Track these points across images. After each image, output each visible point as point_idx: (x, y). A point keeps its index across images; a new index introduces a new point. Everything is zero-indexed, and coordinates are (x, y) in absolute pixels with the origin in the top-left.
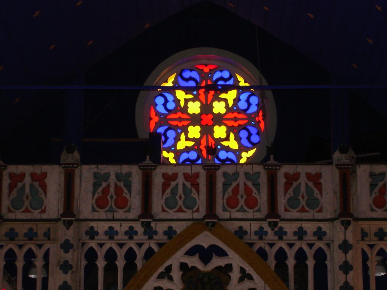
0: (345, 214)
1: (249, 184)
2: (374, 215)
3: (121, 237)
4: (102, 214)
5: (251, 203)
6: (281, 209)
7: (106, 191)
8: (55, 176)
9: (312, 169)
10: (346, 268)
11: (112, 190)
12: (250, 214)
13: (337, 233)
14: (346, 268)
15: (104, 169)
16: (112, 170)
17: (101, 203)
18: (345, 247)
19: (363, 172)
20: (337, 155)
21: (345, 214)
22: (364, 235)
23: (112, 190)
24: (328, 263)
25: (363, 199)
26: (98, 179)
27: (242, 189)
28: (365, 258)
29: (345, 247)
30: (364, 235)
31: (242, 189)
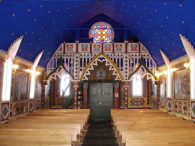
0: (126, 52)
1: (135, 46)
2: (131, 52)
3: (146, 56)
4: (132, 52)
5: (136, 50)
6: (141, 51)
7: (84, 48)
8: (124, 45)
9: (135, 44)
10: (126, 61)
11: (134, 48)
12: (135, 52)
13: (125, 55)
14: (126, 61)
15: (132, 44)
16: (134, 44)
17: (132, 50)
18: (126, 58)
19: (130, 44)
20: (125, 41)
21: (126, 52)
22: (130, 55)
23: (134, 48)
24: (123, 60)
25: (129, 49)
26: (82, 46)
27: (108, 47)
28: (130, 59)
29: (126, 58)
30: (130, 55)
31: (108, 47)
